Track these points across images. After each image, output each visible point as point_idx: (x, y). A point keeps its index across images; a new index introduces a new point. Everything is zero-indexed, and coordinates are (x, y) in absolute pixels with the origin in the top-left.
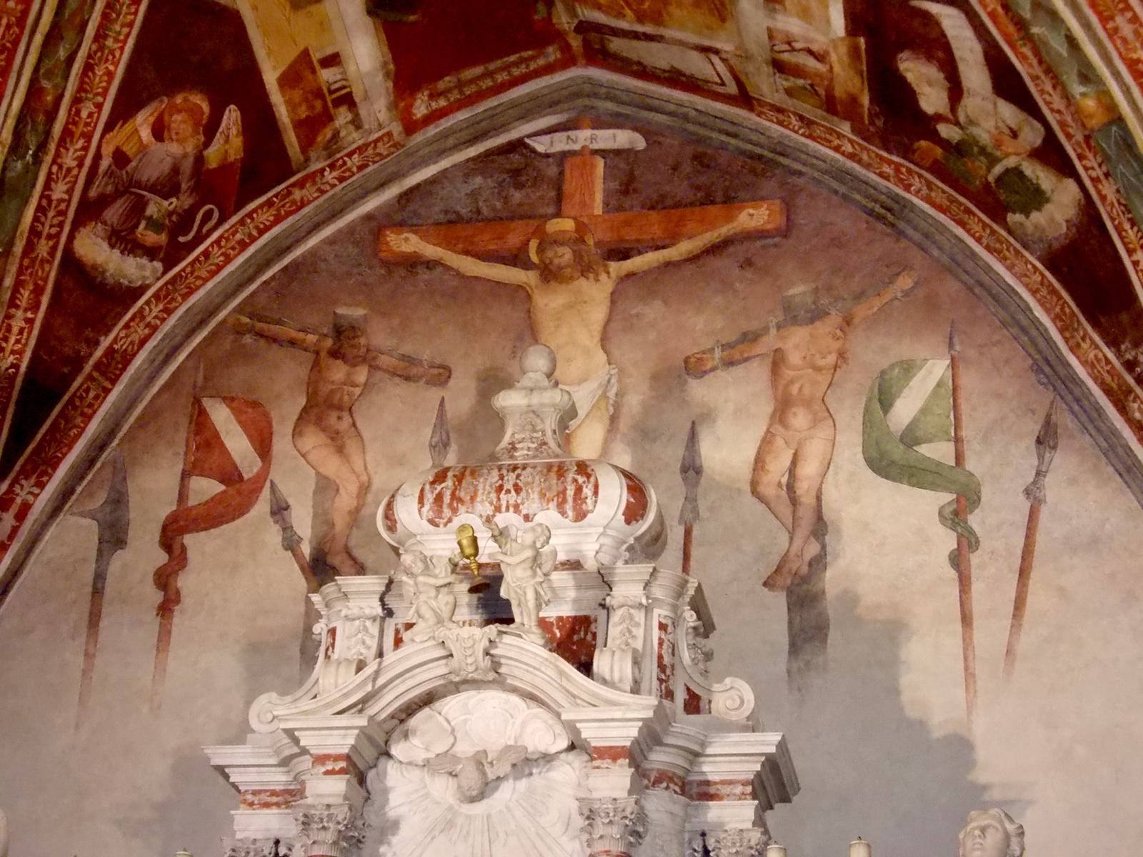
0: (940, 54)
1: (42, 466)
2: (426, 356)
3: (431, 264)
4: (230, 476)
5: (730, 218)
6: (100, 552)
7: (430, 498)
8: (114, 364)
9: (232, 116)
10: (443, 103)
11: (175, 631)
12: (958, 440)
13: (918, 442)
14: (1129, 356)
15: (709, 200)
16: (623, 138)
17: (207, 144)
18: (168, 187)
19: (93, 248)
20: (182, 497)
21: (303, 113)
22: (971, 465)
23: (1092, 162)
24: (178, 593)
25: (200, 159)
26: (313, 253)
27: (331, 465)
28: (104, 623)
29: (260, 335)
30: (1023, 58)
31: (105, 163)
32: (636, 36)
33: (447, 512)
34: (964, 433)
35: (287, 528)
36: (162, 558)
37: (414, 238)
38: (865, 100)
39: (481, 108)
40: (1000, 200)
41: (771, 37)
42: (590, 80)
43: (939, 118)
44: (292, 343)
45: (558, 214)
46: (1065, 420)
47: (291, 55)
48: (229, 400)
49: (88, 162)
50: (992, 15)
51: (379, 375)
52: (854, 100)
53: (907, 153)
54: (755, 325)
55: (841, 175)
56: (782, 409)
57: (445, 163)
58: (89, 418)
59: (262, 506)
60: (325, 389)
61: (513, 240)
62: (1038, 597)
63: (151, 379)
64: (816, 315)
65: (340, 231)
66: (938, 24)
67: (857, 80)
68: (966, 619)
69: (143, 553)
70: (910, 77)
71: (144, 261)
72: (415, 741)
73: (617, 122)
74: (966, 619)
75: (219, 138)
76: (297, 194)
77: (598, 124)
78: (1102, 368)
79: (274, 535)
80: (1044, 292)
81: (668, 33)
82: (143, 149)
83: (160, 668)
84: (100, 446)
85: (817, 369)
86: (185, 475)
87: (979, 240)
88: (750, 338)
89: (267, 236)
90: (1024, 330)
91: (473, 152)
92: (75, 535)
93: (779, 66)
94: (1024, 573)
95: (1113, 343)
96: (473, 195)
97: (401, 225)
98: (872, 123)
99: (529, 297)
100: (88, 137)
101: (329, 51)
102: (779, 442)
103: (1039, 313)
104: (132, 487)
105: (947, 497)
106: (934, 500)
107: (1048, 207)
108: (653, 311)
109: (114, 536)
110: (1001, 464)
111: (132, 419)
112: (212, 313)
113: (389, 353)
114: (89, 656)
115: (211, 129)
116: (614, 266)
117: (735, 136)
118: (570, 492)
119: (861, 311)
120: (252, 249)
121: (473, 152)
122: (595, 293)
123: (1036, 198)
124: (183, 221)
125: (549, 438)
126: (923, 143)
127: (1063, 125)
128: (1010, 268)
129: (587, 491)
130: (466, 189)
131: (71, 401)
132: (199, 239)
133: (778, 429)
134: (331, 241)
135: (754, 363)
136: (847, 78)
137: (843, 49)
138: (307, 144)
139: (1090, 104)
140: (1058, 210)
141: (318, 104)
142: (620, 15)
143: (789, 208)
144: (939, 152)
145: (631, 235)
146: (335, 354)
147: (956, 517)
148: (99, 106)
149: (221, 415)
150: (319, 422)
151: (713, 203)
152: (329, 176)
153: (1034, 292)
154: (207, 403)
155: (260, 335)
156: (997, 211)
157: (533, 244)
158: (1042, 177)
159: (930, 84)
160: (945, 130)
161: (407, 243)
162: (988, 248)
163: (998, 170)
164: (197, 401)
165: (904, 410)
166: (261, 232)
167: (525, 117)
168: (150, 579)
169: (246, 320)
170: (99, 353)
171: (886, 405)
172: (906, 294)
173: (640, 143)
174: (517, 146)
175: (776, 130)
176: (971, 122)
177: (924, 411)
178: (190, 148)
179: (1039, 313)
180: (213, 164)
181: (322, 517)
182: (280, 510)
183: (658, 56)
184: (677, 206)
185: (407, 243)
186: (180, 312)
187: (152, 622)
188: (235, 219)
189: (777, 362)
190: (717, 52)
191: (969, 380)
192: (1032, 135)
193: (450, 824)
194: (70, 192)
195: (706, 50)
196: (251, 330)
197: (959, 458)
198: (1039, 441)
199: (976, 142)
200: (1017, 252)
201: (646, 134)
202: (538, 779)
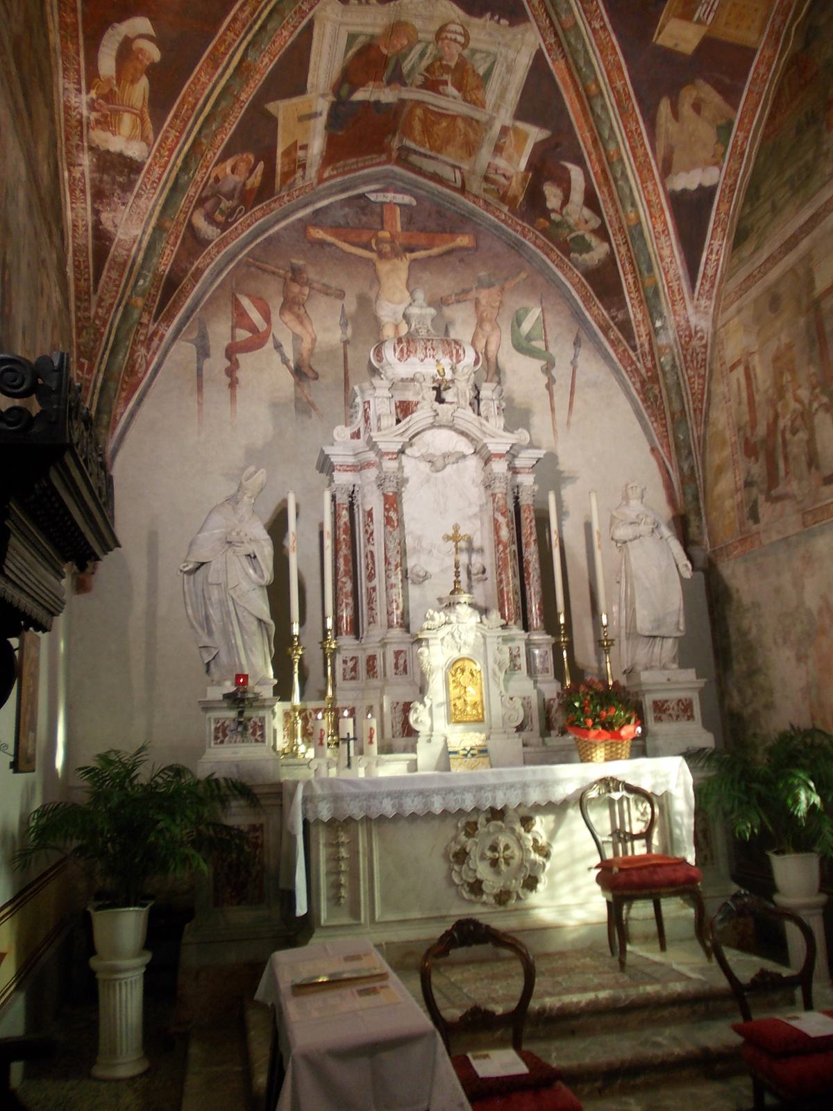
0: (565, 185)
1: (169, 318)
2: (333, 285)
3: (331, 245)
4: (253, 329)
5: (453, 240)
6: (198, 359)
7: (398, 350)
8: (199, 272)
9: (261, 166)
10: (335, 172)
11: (238, 397)
12: (546, 341)
13: (531, 340)
14: (614, 314)
15: (444, 231)
16: (407, 199)
17: (248, 178)
18: (230, 196)
19: (200, 221)
20: (233, 337)
21: (286, 169)
22: (551, 350)
23: (619, 237)
24: (237, 379)
25: (244, 184)
26: (277, 233)
27: (298, 329)
28: (205, 390)
29: (259, 268)
30: (602, 192)
31: (211, 180)
32: (425, 156)
33: (405, 356)
34: (548, 338)
35: (282, 355)
36: (228, 364)
37: (321, 232)
38: (521, 199)
39: (347, 177)
40: (569, 246)
41: (489, 166)
42: (392, 171)
43: (553, 211)
44: (274, 273)
45: (383, 229)
46: (584, 337)
47: (290, 142)
48: (249, 296)
49: (205, 180)
50: (595, 174)
51: (313, 292)
52: (515, 198)
53: (531, 223)
54: (466, 287)
55: (497, 228)
56: (480, 323)
57: (332, 200)
58: (187, 297)
59: (270, 344)
60: (291, 295)
61: (365, 238)
62: (577, 404)
63: (212, 283)
64: (491, 285)
65: (288, 225)
66: (569, 173)
67: (521, 190)
68: (553, 409)
69: (217, 363)
70: (546, 192)
71: (215, 228)
72: (415, 448)
73: (403, 191)
74: (553, 409)
75: (253, 175)
76: (273, 205)
77: (396, 191)
78: (600, 318)
79: (277, 357)
80: (579, 286)
81: (440, 157)
82: (226, 176)
83: (234, 411)
84: (191, 310)
85: (493, 308)
86: (233, 328)
87: (553, 262)
88: (465, 292)
89: (258, 223)
90: (568, 300)
91: (344, 196)
92: (184, 351)
93: (486, 179)
94: (572, 393)
95: (608, 309)
96: (345, 216)
97: (316, 225)
98: (520, 207)
99: (374, 265)
100: (207, 168)
101: (305, 143)
102: (480, 336)
103: (574, 293)
104: (209, 331)
105: (544, 363)
106: (538, 364)
107: (592, 253)
108: (426, 276)
109: (204, 352)
110: (562, 351)
111: (205, 300)
112: (235, 256)
113: (318, 282)
114: (200, 404)
115: (251, 171)
116: (408, 255)
117: (454, 205)
118: (454, 352)
119: (507, 286)
120: (252, 228)
121: (344, 196)
122: (403, 265)
123: (588, 248)
124: (231, 213)
125: (430, 328)
126: (542, 220)
127: (610, 221)
128: (565, 275)
129: (461, 352)
130: (342, 213)
131: (181, 290)
132: (235, 221)
133: (479, 330)
134: (285, 228)
135: (468, 303)
136: (516, 188)
137: (520, 177)
138: (283, 182)
139: (632, 215)
140: (599, 251)
141: (292, 166)
142: (424, 146)
143: (477, 240)
144: (547, 224)
145: (414, 242)
146: (294, 280)
147: (547, 370)
148: (215, 154)
149: (246, 302)
150: (291, 310)
151: (446, 232)
152: (286, 199)
153: (574, 285)
154: (239, 296)
155: (259, 268)
156: (567, 252)
157: (373, 242)
158: (593, 241)
159: (555, 196)
160: (553, 216)
161: (319, 234)
162: (557, 265)
163: (573, 235)
164: (234, 295)
165: (526, 327)
166: (256, 220)
167: (365, 183)
168: (224, 372)
169: (251, 260)
170: (193, 268)
171: (519, 325)
172: (524, 280)
173: (414, 203)
174: (362, 196)
175: (471, 204)
176: (568, 214)
177: (533, 328)
178: (242, 179)
179: (574, 293)
180: (248, 187)
181: (297, 350)
182: (278, 346)
183: (429, 166)
184: (432, 231)
185: (319, 234)
186: (222, 253)
187: (227, 391)
188: (249, 214)
189: (477, 303)
190: (460, 168)
191: (549, 318)
192: (595, 223)
193: (428, 481)
194: (195, 193)
195: (454, 167)
196: (254, 265)
197: (547, 347)
198: (575, 344)
199: (567, 222)
200: (570, 269)
201: (416, 198)
202: (461, 464)
